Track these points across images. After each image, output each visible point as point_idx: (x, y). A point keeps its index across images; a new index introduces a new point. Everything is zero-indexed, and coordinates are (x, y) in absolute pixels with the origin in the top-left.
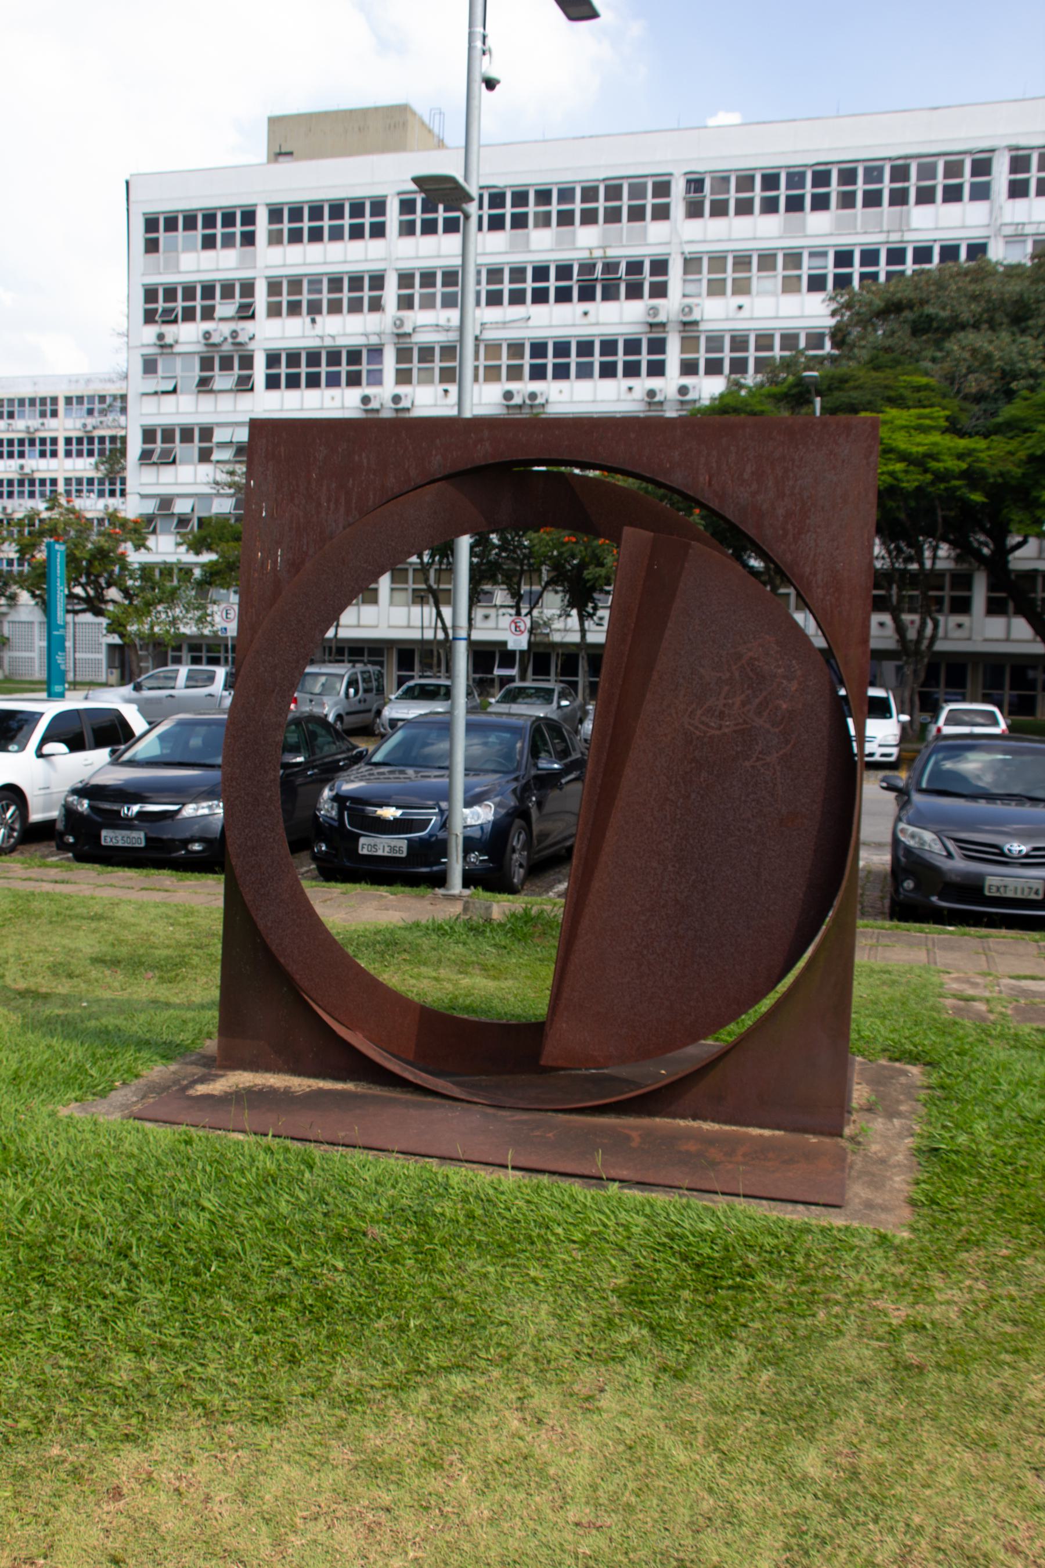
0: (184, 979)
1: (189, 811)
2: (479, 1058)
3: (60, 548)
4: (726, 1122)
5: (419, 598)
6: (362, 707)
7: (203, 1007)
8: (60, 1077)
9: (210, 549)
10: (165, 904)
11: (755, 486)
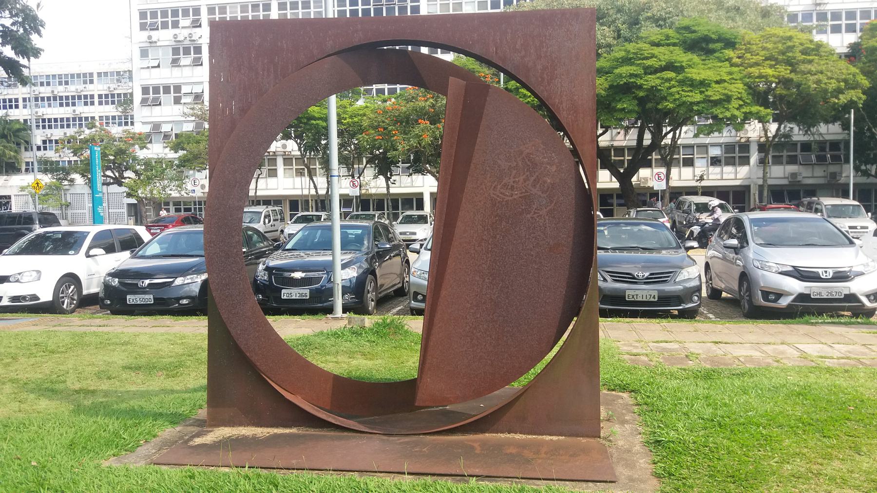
0: (182, 374)
1: (179, 281)
2: (377, 405)
3: (97, 149)
4: (529, 434)
5: (300, 173)
6: (273, 229)
7: (195, 390)
8: (102, 441)
9: (183, 149)
10: (167, 334)
11: (523, 53)
